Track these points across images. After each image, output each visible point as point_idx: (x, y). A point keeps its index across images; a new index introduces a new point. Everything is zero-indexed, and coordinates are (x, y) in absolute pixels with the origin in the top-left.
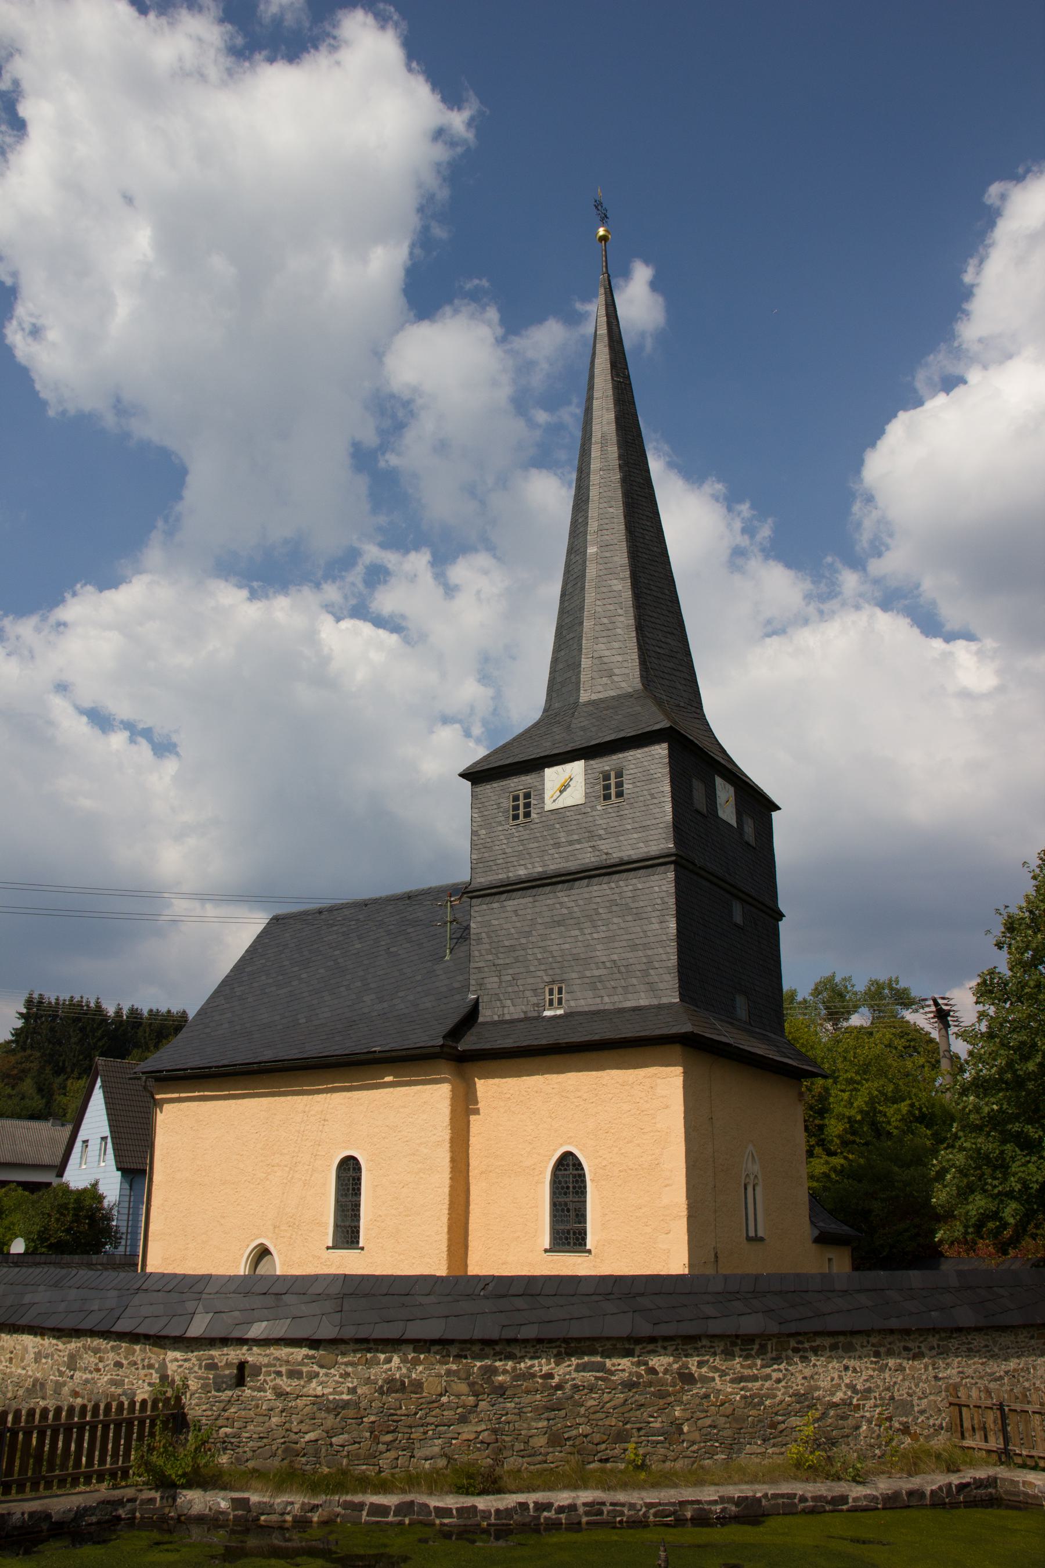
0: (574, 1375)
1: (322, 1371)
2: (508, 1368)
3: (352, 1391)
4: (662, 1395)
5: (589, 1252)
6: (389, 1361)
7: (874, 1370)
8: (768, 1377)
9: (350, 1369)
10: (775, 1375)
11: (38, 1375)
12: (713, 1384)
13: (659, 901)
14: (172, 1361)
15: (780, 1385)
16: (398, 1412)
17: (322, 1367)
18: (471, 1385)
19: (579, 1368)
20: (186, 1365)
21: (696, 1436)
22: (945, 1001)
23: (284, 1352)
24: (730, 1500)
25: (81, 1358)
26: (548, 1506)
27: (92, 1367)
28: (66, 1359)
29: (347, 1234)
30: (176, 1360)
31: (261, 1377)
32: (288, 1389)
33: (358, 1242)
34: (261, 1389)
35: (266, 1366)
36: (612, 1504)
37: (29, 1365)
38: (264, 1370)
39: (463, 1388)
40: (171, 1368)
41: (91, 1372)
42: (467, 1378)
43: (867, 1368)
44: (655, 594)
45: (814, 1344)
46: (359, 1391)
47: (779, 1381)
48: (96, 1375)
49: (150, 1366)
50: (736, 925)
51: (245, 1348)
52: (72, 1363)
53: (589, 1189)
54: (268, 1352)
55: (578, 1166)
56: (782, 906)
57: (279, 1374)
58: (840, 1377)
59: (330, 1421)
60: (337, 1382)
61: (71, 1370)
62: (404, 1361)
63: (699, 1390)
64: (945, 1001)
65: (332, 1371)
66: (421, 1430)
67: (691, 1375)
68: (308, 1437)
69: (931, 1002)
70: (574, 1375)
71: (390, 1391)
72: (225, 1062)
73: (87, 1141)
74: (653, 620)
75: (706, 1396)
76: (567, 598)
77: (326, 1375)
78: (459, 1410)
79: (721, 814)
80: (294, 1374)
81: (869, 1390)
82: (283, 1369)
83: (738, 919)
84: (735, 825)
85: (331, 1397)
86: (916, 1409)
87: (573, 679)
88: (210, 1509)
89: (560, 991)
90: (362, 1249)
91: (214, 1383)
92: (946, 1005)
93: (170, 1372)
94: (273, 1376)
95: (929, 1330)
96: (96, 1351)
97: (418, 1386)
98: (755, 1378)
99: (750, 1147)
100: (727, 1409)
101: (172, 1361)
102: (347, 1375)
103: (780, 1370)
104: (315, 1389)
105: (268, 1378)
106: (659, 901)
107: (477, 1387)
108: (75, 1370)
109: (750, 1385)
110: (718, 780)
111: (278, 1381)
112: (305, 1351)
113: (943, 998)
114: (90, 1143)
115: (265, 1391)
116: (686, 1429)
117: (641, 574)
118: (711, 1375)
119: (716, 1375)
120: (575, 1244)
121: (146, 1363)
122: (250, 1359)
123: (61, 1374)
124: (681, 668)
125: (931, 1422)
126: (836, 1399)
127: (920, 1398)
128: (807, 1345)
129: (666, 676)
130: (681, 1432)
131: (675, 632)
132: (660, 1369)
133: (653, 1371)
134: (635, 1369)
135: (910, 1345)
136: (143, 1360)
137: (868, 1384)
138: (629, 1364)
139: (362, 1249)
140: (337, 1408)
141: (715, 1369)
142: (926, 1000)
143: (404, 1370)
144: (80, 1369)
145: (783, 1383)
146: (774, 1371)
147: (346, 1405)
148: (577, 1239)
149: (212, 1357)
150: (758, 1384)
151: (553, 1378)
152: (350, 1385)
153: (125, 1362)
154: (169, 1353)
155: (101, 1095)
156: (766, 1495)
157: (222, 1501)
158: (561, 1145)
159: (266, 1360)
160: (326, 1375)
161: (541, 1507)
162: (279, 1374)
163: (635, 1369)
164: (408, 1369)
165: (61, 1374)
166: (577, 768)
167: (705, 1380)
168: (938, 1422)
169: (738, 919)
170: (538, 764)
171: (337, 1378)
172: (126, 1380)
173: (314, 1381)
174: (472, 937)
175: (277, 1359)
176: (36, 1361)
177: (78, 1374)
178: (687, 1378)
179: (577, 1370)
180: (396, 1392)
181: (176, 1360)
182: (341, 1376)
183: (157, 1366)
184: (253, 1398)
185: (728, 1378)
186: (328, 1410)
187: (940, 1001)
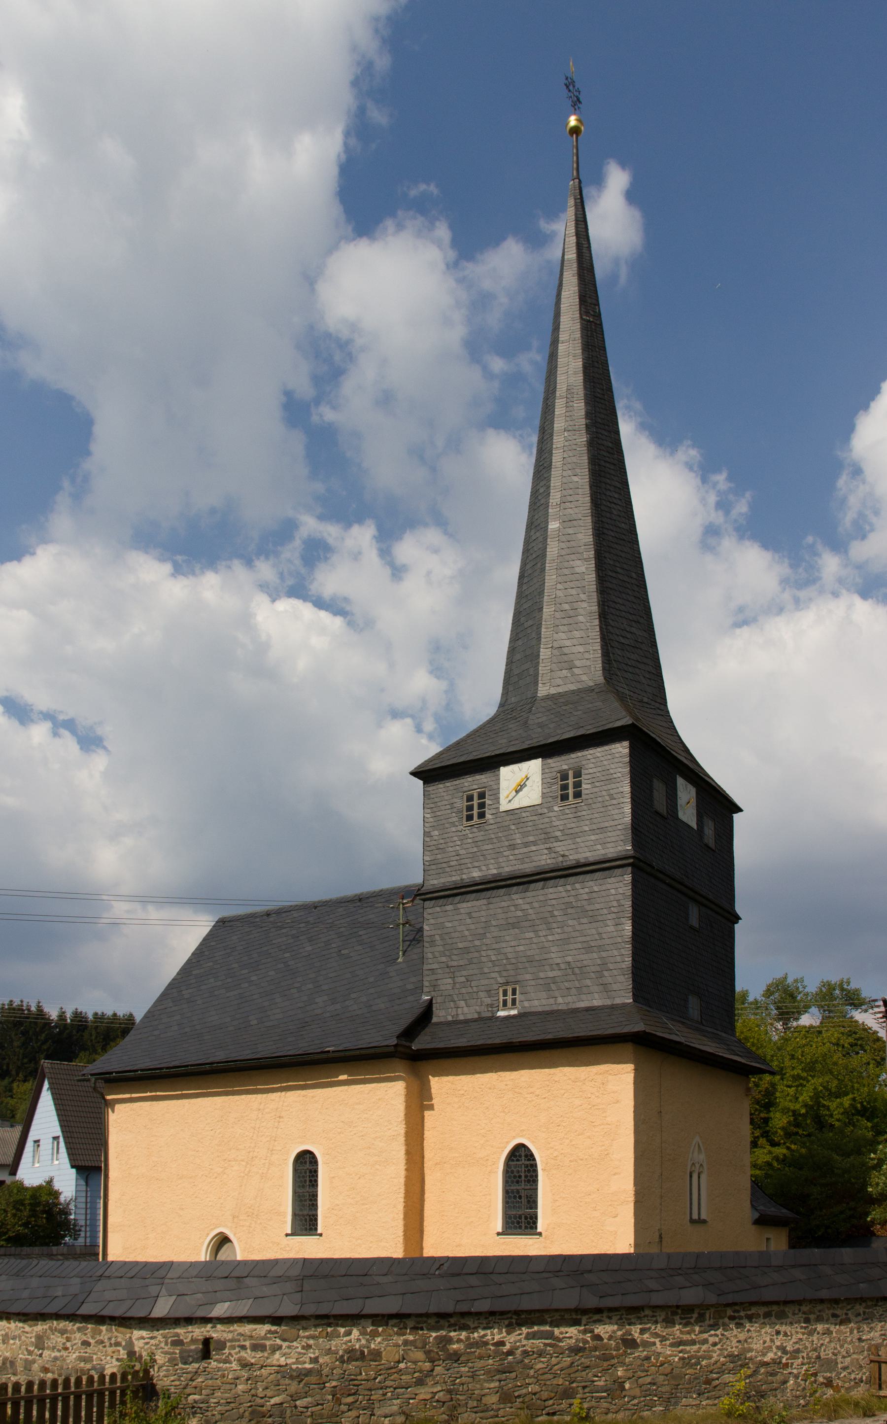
0: (524, 1342)
3: (315, 1360)
5: (540, 1234)
6: (349, 1333)
8: (705, 1341)
9: (311, 1342)
10: (712, 1340)
12: (654, 1348)
14: (138, 1339)
15: (716, 1348)
16: (359, 1377)
17: (284, 1340)
18: (428, 1353)
20: (153, 1342)
25: (49, 1338)
27: (60, 1346)
28: (33, 1340)
30: (143, 1338)
31: (227, 1351)
32: (253, 1361)
33: (316, 1229)
34: (226, 1361)
38: (228, 1344)
39: (420, 1355)
40: (138, 1345)
41: (59, 1351)
42: (424, 1347)
43: (797, 1333)
44: (621, 577)
45: (749, 1313)
46: (321, 1360)
47: (715, 1344)
49: (118, 1344)
50: (691, 927)
51: (210, 1325)
52: (40, 1342)
55: (530, 1156)
56: (739, 909)
57: (243, 1347)
58: (772, 1341)
60: (300, 1353)
61: (39, 1349)
63: (641, 1353)
65: (295, 1344)
70: (524, 1342)
71: (350, 1360)
74: (618, 606)
75: (647, 1358)
76: (526, 580)
77: (289, 1347)
78: (416, 1375)
81: (798, 1351)
82: (247, 1343)
83: (694, 921)
84: (695, 827)
85: (294, 1366)
86: (840, 1366)
87: (531, 671)
89: (514, 993)
90: (321, 1235)
93: (137, 1349)
94: (237, 1349)
96: (63, 1332)
97: (376, 1355)
100: (667, 1368)
101: (138, 1339)
102: (309, 1347)
103: (716, 1335)
105: (233, 1352)
108: (43, 1349)
109: (688, 1348)
110: (680, 781)
111: (243, 1354)
115: (230, 1363)
117: (607, 555)
118: (652, 1340)
120: (526, 1228)
121: (113, 1341)
123: (30, 1353)
127: (844, 1357)
128: (742, 1314)
129: (631, 669)
131: (641, 620)
132: (605, 1336)
133: (598, 1338)
134: (581, 1336)
135: (838, 1312)
138: (576, 1332)
139: (321, 1235)
140: (300, 1376)
141: (656, 1335)
143: (363, 1342)
144: (48, 1348)
145: (719, 1346)
146: (711, 1336)
147: (309, 1372)
149: (177, 1335)
150: (695, 1347)
152: (312, 1356)
153: (92, 1341)
159: (230, 1336)
160: (289, 1347)
162: (243, 1347)
163: (581, 1336)
164: (367, 1340)
165: (30, 1353)
166: (534, 766)
167: (646, 1344)
169: (694, 921)
171: (299, 1350)
172: (95, 1357)
173: (278, 1353)
177: (46, 1353)
179: (527, 1338)
181: (143, 1338)
182: (303, 1347)
183: (124, 1343)
184: (219, 1369)
185: (668, 1342)
186: (292, 1378)
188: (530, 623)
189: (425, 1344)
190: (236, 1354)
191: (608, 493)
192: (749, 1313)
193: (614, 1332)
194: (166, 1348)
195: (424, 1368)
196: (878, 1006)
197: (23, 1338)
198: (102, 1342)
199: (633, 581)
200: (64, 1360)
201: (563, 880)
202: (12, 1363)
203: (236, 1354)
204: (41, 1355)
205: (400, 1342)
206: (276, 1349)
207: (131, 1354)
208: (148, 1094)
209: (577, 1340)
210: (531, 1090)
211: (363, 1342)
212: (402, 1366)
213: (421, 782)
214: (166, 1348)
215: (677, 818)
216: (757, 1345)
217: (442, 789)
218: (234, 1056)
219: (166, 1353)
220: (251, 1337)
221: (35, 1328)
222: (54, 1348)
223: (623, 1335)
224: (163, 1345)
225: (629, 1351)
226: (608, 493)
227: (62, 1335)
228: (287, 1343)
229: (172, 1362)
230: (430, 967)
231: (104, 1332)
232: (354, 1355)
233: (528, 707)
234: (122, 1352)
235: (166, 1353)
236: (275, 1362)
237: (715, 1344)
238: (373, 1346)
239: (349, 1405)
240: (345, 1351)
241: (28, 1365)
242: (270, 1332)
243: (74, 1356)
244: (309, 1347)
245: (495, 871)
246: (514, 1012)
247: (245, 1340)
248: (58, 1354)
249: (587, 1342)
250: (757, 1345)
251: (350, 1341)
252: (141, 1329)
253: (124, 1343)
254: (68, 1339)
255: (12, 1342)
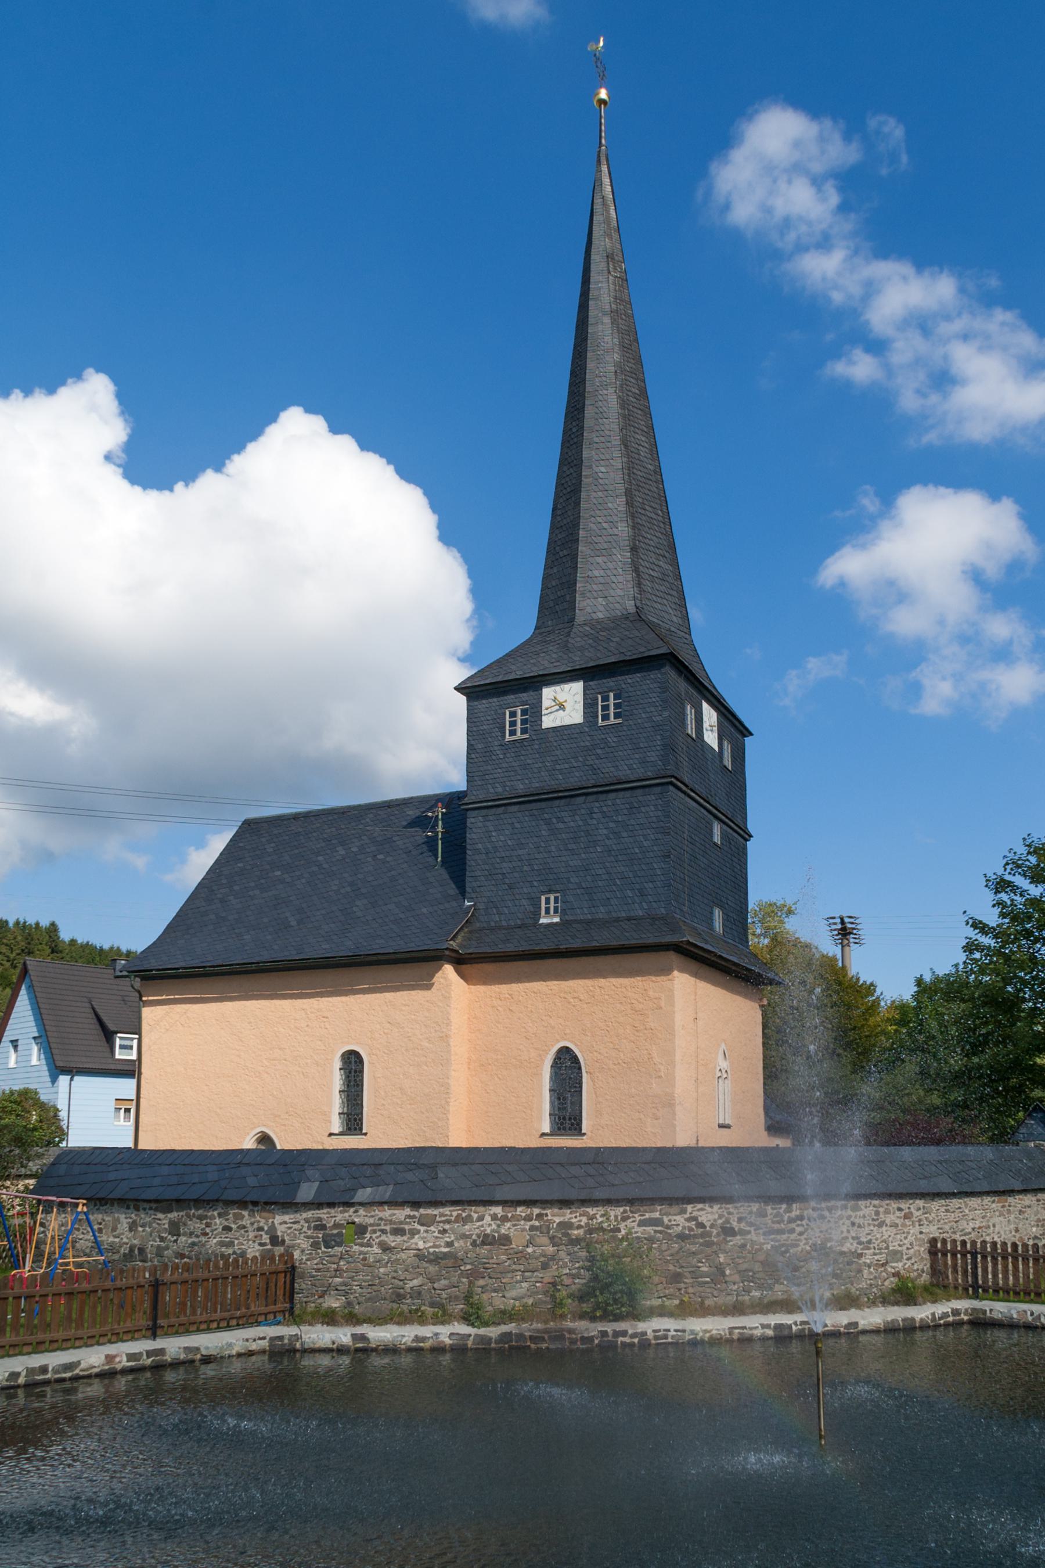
0: (636, 1229)
1: (422, 1229)
2: (582, 1224)
3: (449, 1244)
4: (709, 1244)
5: (584, 1134)
6: (481, 1218)
7: (874, 1226)
8: (792, 1231)
9: (447, 1227)
10: (799, 1229)
11: (135, 1242)
12: (749, 1237)
13: (654, 819)
14: (281, 1224)
15: (802, 1238)
16: (491, 1261)
17: (422, 1225)
18: (552, 1239)
19: (641, 1224)
20: (295, 1226)
21: (736, 1278)
22: (852, 920)
23: (387, 1213)
24: (768, 1326)
25: (185, 1224)
26: (624, 1333)
27: (199, 1232)
28: (166, 1226)
29: (353, 1122)
30: (286, 1223)
31: (368, 1235)
32: (393, 1244)
33: (361, 1129)
34: (370, 1245)
35: (371, 1225)
36: (676, 1331)
37: (123, 1234)
38: (370, 1229)
39: (545, 1240)
40: (280, 1230)
41: (197, 1236)
42: (548, 1233)
43: (869, 1225)
44: (649, 514)
45: (829, 1204)
46: (456, 1244)
47: (801, 1234)
48: (203, 1239)
49: (260, 1229)
50: (715, 844)
51: (352, 1210)
52: (175, 1229)
53: (584, 1080)
54: (373, 1213)
55: (575, 1060)
56: (751, 827)
57: (383, 1232)
58: (848, 1231)
59: (432, 1269)
60: (437, 1237)
61: (173, 1236)
62: (494, 1217)
63: (738, 1240)
64: (852, 920)
65: (432, 1228)
66: (510, 1275)
67: (733, 1229)
68: (411, 1284)
69: (838, 921)
70: (636, 1229)
71: (483, 1243)
72: (220, 962)
73: (17, 1041)
74: (647, 541)
75: (744, 1246)
76: (559, 512)
77: (427, 1231)
78: (542, 1259)
79: (706, 739)
80: (398, 1231)
81: (870, 1242)
82: (388, 1228)
83: (717, 839)
84: (717, 749)
85: (431, 1250)
86: (905, 1257)
87: (568, 598)
88: (334, 1343)
89: (556, 901)
90: (365, 1134)
91: (324, 1241)
92: (852, 923)
93: (279, 1234)
94: (378, 1233)
95: (916, 1194)
96: (200, 1218)
97: (506, 1240)
98: (781, 1232)
99: (723, 1046)
100: (761, 1257)
101: (281, 1224)
102: (445, 1231)
103: (802, 1225)
104: (416, 1244)
105: (374, 1236)
106: (654, 819)
107: (556, 1240)
108: (179, 1235)
109: (778, 1237)
110: (705, 706)
111: (384, 1238)
112: (408, 1211)
113: (850, 917)
114: (19, 1043)
115: (372, 1247)
116: (728, 1272)
117: (637, 493)
118: (748, 1228)
119: (752, 1229)
120: (570, 1129)
121: (256, 1226)
122: (356, 1220)
123: (162, 1239)
124: (671, 592)
125: (915, 1267)
126: (845, 1249)
127: (908, 1249)
128: (823, 1205)
129: (659, 600)
130: (723, 1274)
131: (667, 555)
132: (708, 1224)
133: (701, 1225)
134: (687, 1224)
135: (903, 1206)
136: (252, 1224)
137: (869, 1237)
138: (682, 1220)
139: (365, 1134)
140: (436, 1259)
141: (751, 1224)
142: (834, 918)
143: (494, 1227)
144: (185, 1234)
145: (805, 1236)
146: (798, 1225)
147: (445, 1256)
148: (572, 1124)
149: (320, 1219)
150: (785, 1236)
151: (620, 1231)
152: (448, 1240)
153: (234, 1226)
154: (277, 1217)
155: (26, 997)
156: (795, 1323)
157: (343, 1335)
158: (558, 1041)
159: (371, 1221)
160: (427, 1231)
161: (617, 1334)
162: (383, 1232)
163: (687, 1224)
164: (499, 1226)
165: (162, 1239)
166: (575, 689)
167: (742, 1232)
168: (920, 1267)
169: (717, 839)
170: (535, 683)
171: (436, 1234)
172: (236, 1242)
173: (416, 1236)
174: (468, 847)
175: (381, 1219)
176: (131, 1230)
177: (183, 1239)
178: (728, 1231)
179: (639, 1225)
180: (489, 1244)
181: (286, 1223)
182: (440, 1232)
183: (266, 1228)
184: (361, 1253)
185: (761, 1231)
186: (430, 1261)
187: (847, 920)
188: (565, 552)
189: (548, 1229)
190: (377, 1237)
191: (637, 436)
192: (829, 1204)
193: (715, 1220)
194: (309, 1233)
195: (548, 1253)
196: (835, 924)
197: (154, 1225)
198: (244, 1227)
199: (660, 519)
200: (204, 1245)
201: (605, 795)
202: (141, 1250)
203: (377, 1237)
204: (176, 1241)
205: (527, 1227)
206: (413, 1233)
207: (275, 1240)
208: (696, 951)
209: (684, 1228)
210: (576, 995)
211: (494, 1227)
212: (530, 1250)
213: (465, 698)
214: (309, 1233)
215: (703, 741)
216: (836, 1236)
217: (483, 704)
218: (280, 956)
219: (308, 1237)
220: (391, 1222)
221: (169, 1215)
222: (191, 1234)
223: (724, 1223)
224: (305, 1229)
225: (729, 1239)
226: (637, 436)
227: (201, 1220)
228: (425, 1228)
229: (315, 1245)
230: (473, 874)
231: (247, 1217)
232: (487, 1240)
233: (566, 630)
234: (265, 1236)
235: (308, 1237)
236: (413, 1246)
237: (801, 1234)
238: (503, 1231)
239: (482, 1287)
240: (479, 1236)
241: (159, 1252)
242: (409, 1217)
243: (215, 1241)
244: (445, 1231)
245: (537, 785)
246: (556, 920)
247: (385, 1225)
248: (196, 1240)
249: (692, 1230)
250: (836, 1236)
251: (482, 1226)
252: (284, 1213)
253: (266, 1228)
254: (208, 1225)
255: (140, 1229)
